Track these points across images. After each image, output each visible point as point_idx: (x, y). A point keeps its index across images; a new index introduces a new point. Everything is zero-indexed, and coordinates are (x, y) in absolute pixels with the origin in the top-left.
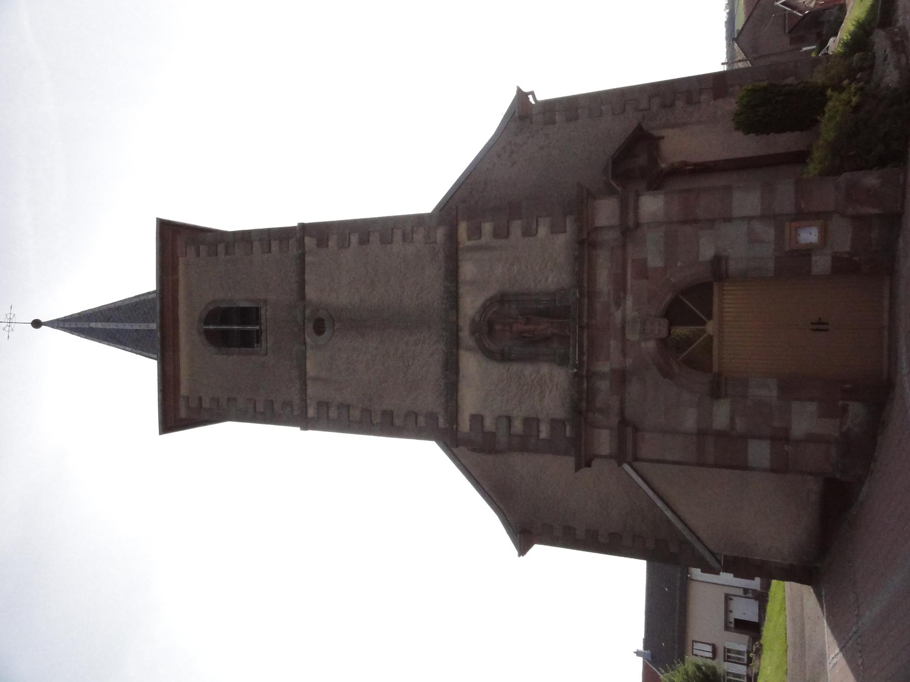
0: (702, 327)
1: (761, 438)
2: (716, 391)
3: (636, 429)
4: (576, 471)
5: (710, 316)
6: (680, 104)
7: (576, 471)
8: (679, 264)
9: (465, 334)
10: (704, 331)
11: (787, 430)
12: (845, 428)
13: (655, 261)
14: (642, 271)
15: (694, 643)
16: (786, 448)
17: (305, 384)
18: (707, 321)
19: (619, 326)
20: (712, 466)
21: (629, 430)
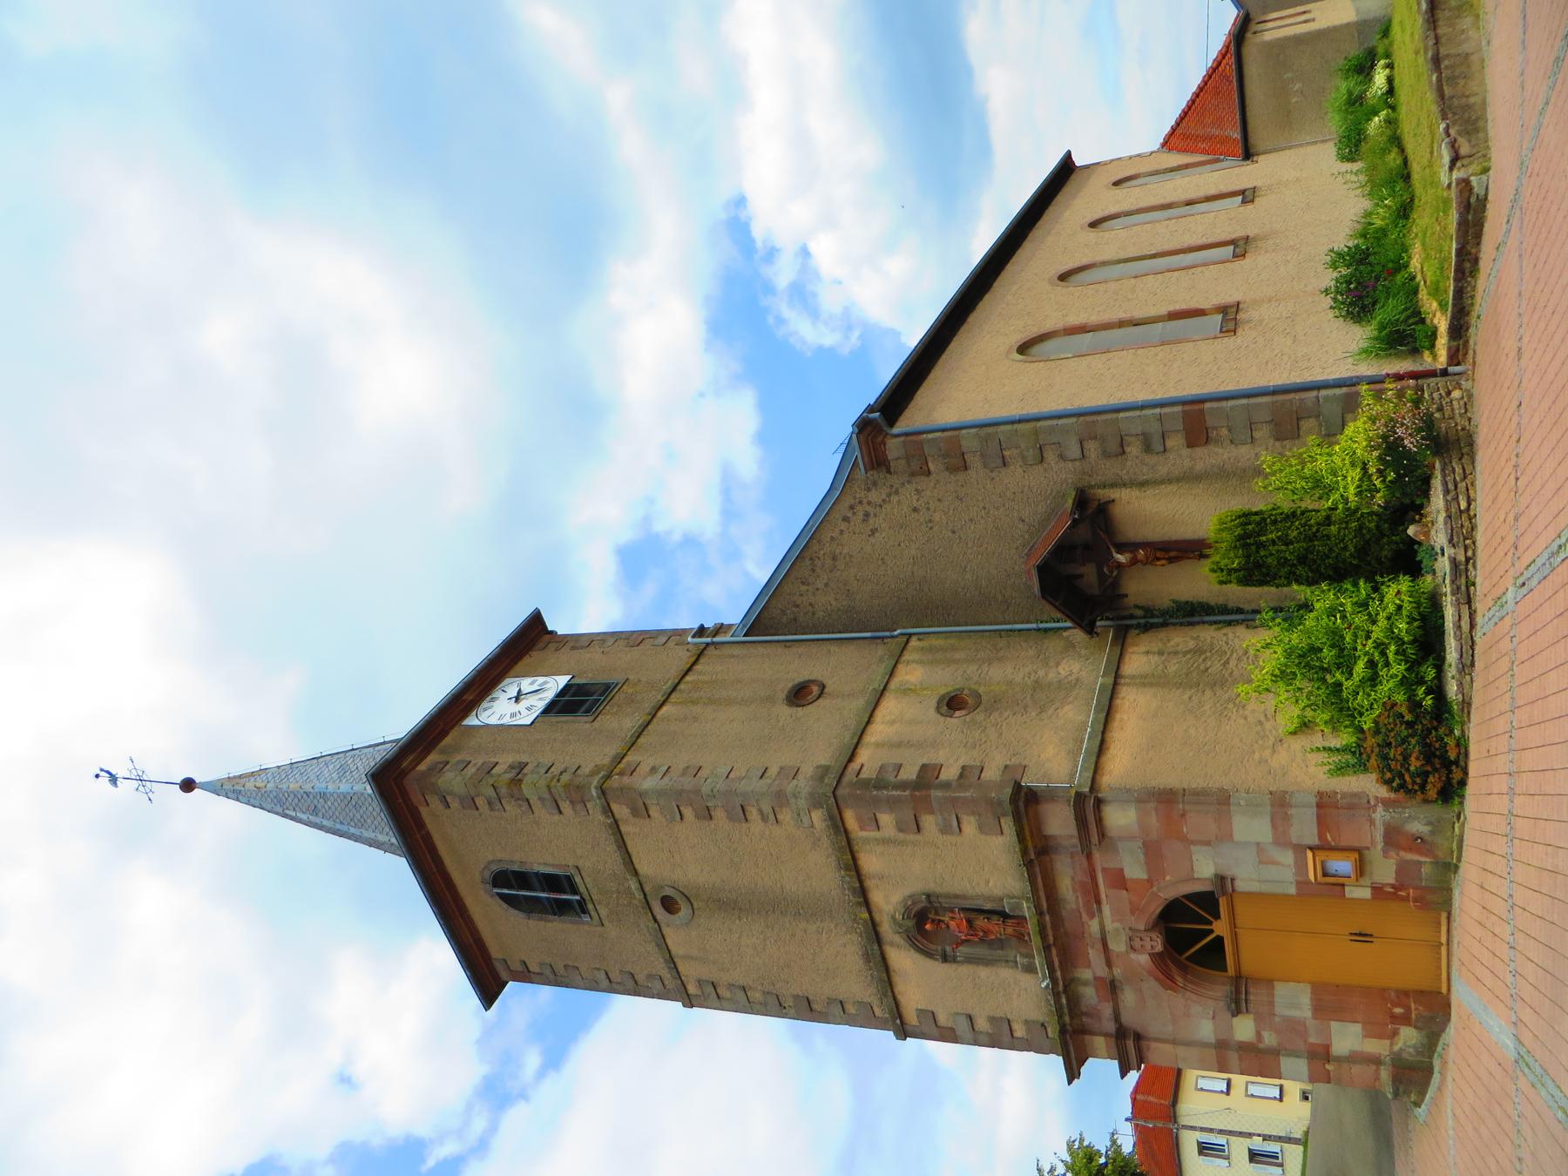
0: (1212, 920)
1: (1295, 1054)
2: (1237, 1006)
3: (1138, 1037)
4: (1070, 1082)
5: (1217, 917)
6: (1134, 449)
7: (1070, 1082)
8: (1168, 878)
9: (886, 929)
10: (1210, 923)
11: (1327, 1048)
12: (1396, 1048)
13: (1135, 870)
14: (1119, 880)
15: (1278, 1097)
16: (1327, 1067)
17: (519, 773)
18: (1211, 928)
19: (1099, 936)
20: (1402, 150)
21: (1130, 1044)
